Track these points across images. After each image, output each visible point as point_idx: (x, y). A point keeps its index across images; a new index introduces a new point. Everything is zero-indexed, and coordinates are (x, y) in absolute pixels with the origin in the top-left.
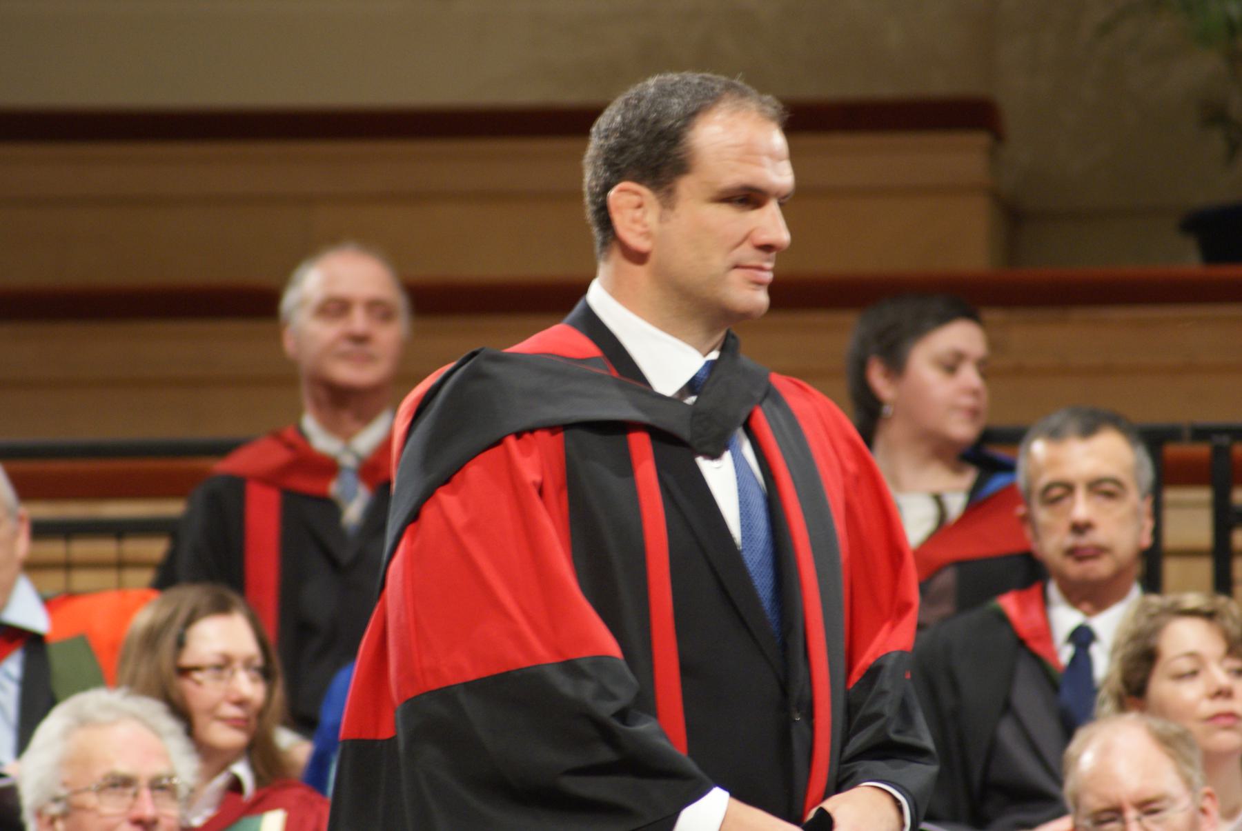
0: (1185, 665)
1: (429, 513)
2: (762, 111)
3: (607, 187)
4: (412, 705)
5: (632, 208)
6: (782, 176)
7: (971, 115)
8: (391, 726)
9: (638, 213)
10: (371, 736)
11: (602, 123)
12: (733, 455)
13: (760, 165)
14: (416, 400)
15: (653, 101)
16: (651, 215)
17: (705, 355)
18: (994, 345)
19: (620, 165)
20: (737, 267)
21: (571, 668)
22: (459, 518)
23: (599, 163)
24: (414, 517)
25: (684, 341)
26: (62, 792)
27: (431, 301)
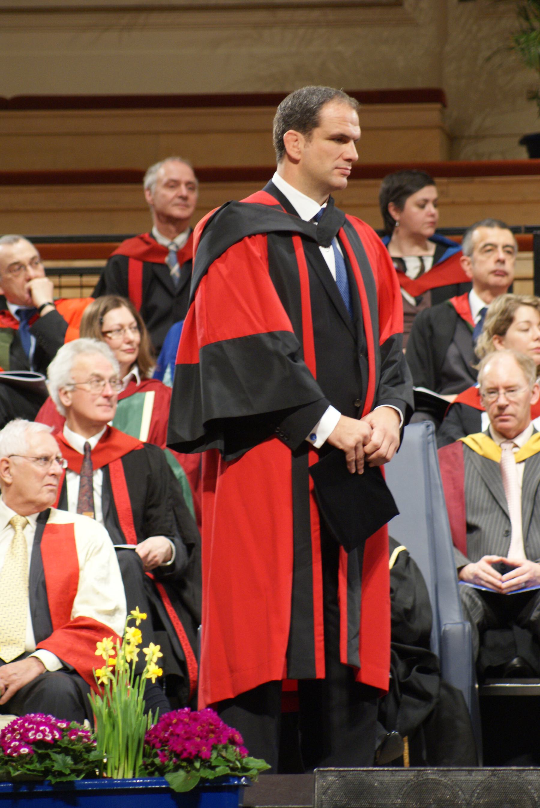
0: (525, 326)
1: (212, 270)
2: (350, 104)
3: (284, 132)
4: (206, 349)
5: (294, 141)
6: (356, 131)
7: (434, 96)
8: (198, 358)
9: (296, 144)
10: (189, 362)
11: (283, 104)
12: (333, 247)
13: (347, 126)
14: (204, 222)
15: (305, 97)
16: (301, 144)
17: (321, 205)
18: (441, 193)
19: (289, 122)
20: (337, 168)
21: (271, 335)
22: (224, 271)
23: (281, 121)
24: (206, 272)
25: (312, 198)
26: (72, 382)
27: (205, 176)
